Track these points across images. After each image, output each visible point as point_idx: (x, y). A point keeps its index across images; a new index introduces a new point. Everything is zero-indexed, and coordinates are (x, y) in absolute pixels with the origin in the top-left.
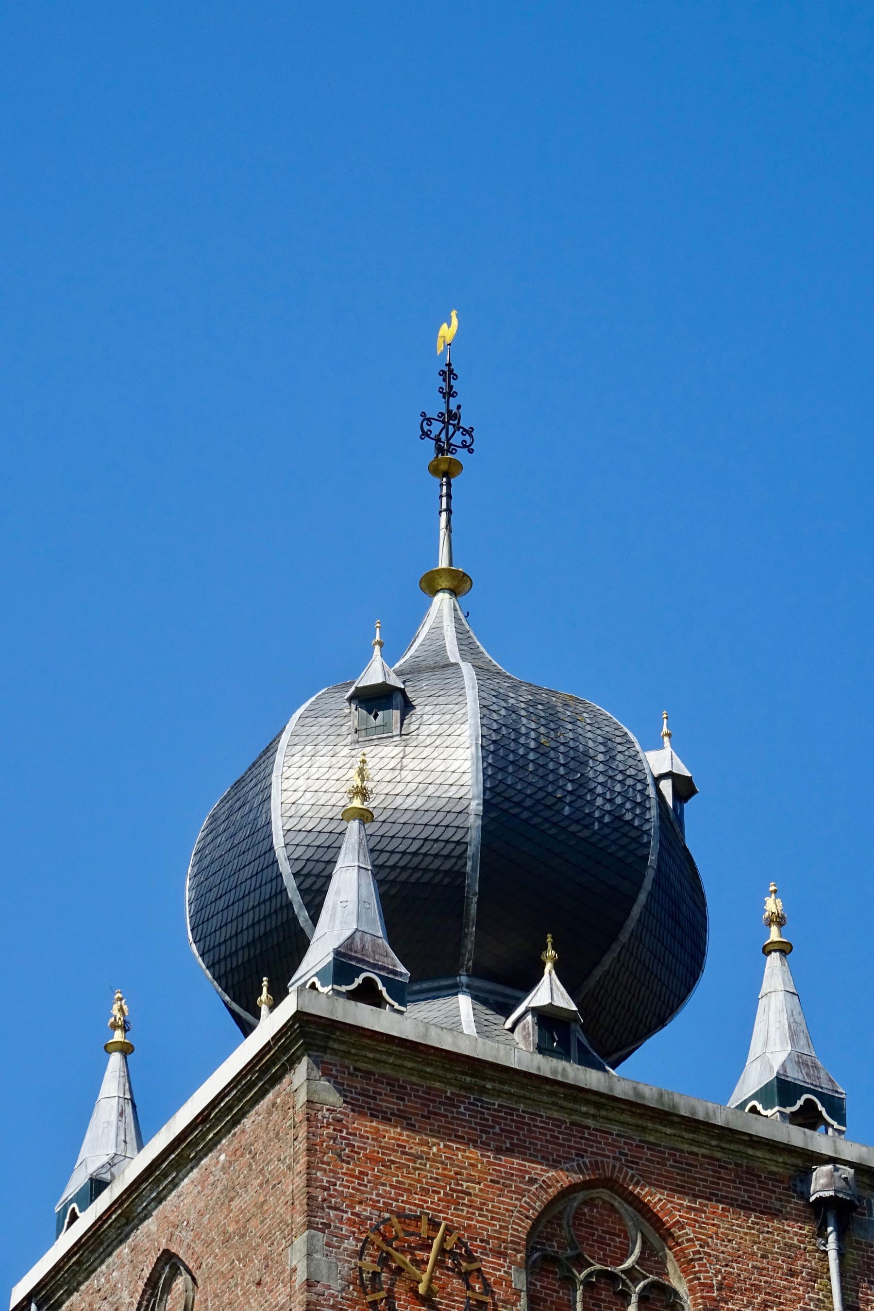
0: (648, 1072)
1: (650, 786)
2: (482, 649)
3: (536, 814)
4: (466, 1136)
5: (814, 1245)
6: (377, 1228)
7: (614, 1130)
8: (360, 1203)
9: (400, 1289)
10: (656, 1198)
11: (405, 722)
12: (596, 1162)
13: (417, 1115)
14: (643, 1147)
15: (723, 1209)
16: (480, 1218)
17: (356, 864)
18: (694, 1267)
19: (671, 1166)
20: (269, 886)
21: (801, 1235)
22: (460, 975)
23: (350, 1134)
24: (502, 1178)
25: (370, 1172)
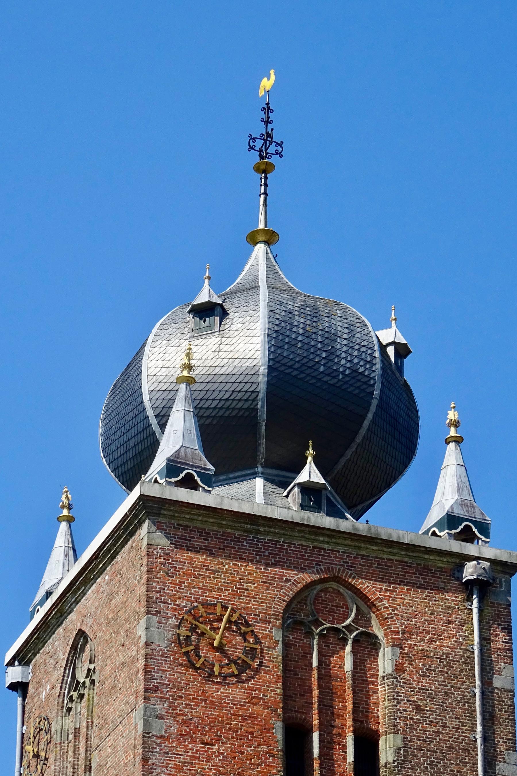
0: (384, 518)
1: (377, 351)
2: (283, 276)
3: (302, 372)
4: (247, 558)
5: (464, 606)
6: (190, 611)
7: (340, 549)
8: (180, 598)
9: (203, 644)
10: (365, 585)
11: (223, 323)
12: (328, 568)
13: (216, 548)
14: (358, 558)
15: (407, 589)
16: (254, 603)
17: (184, 408)
18: (388, 622)
19: (376, 567)
20: (142, 423)
21: (456, 601)
22: (258, 467)
23: (174, 561)
24: (269, 580)
25: (186, 582)
